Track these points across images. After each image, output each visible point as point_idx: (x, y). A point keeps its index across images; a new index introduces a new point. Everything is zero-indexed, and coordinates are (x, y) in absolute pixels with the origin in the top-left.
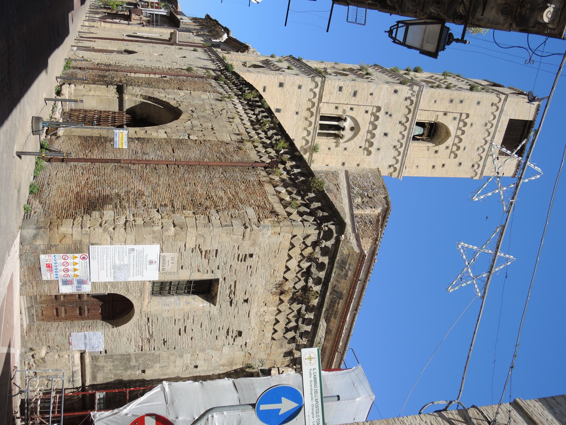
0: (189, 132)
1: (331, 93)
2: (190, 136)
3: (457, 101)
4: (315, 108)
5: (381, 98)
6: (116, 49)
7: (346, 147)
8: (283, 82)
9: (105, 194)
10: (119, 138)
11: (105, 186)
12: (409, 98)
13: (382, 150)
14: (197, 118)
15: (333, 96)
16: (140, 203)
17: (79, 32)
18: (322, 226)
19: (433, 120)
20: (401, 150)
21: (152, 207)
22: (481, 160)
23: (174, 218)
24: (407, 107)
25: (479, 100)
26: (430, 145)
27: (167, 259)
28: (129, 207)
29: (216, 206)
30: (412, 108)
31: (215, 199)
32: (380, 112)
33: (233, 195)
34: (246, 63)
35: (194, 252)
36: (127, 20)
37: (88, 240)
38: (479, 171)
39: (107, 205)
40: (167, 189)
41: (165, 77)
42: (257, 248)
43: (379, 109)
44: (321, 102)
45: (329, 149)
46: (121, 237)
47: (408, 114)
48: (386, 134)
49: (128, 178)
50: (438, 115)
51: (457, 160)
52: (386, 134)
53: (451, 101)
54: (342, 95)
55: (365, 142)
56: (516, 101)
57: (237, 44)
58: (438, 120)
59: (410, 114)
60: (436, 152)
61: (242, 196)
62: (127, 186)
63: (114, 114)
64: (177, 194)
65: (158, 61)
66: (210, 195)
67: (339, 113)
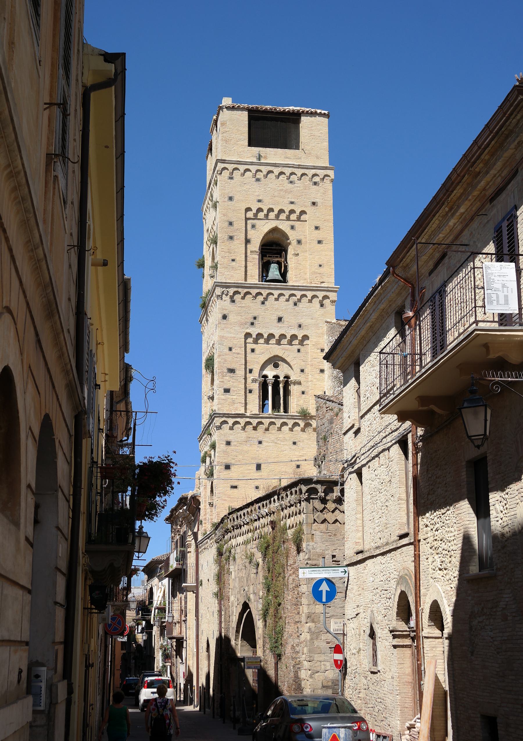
1: (233, 402)
4: (251, 420)
5: (234, 336)
12: (232, 298)
13: (301, 321)
15: (237, 399)
20: (299, 294)
24: (243, 298)
25: (227, 199)
26: (291, 251)
27: (337, 628)
30: (243, 291)
32: (251, 333)
35: (330, 606)
36: (182, 642)
37: (319, 690)
38: (322, 173)
42: (327, 552)
43: (248, 335)
44: (245, 415)
45: (303, 393)
46: (316, 665)
48: (280, 319)
50: (251, 252)
52: (280, 319)
54: (234, 387)
67: (256, 387)
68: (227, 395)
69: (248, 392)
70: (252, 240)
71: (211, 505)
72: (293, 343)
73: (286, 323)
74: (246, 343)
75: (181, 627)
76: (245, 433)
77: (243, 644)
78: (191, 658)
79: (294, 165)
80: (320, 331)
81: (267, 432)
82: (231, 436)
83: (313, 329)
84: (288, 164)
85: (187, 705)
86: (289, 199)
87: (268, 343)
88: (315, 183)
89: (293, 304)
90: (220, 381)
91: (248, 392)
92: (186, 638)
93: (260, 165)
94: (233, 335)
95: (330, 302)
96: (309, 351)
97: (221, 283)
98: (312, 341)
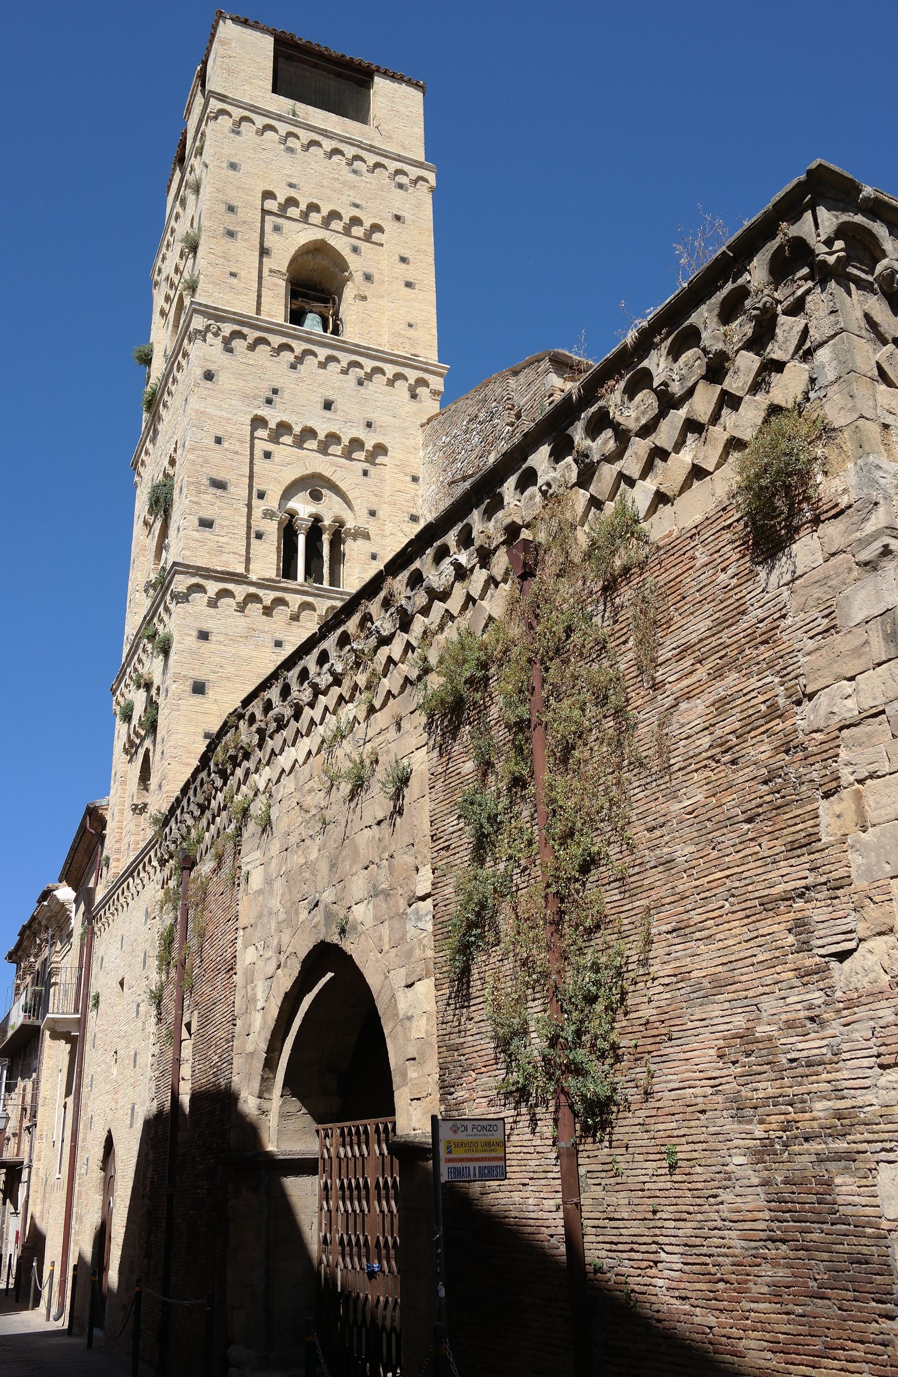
0: (402, 903)
1: (220, 550)
2: (420, 893)
3: (229, 220)
4: (261, 593)
5: (229, 416)
6: (99, 1198)
7: (365, 512)
8: (190, 683)
9: (767, 1215)
10: (471, 1160)
11: (714, 1216)
13: (373, 416)
14: (339, 886)
15: (228, 544)
16: (800, 1046)
17: (48, 1319)
18: (831, 260)
19: (283, 283)
20: (368, 364)
21: (821, 985)
22: (383, 166)
23: (879, 875)
24: (252, 347)
25: (225, 165)
26: (349, 292)
28: (838, 1093)
29: (774, 712)
30: (253, 335)
31: (728, 729)
32: (267, 418)
33: (700, 662)
34: (136, 805)
36: (20, 1172)
38: (414, 172)
39: (840, 1200)
40: (698, 935)
41: (188, 1026)
43: (258, 422)
44: (246, 577)
47: (269, 344)
49: (654, 1112)
50: (271, 271)
51: (389, 225)
52: (328, 405)
53: (231, 234)
54: (224, 518)
55: (354, 462)
56: (224, 75)
57: (81, 849)
58: (284, 270)
59: (269, 339)
60: (368, 277)
61: (701, 625)
62: (703, 1112)
63: (333, 1193)
64: (721, 889)
65: (135, 1062)
66: (709, 754)
67: (271, 528)
68: (206, 533)
69: (253, 535)
70: (274, 251)
71: (138, 811)
72: (354, 456)
73: (340, 413)
74: (253, 438)
75: (19, 1144)
76: (243, 619)
77: (287, 1108)
78: (39, 1201)
79: (361, 142)
80: (411, 442)
81: (295, 623)
82: (211, 620)
83: (396, 435)
84: (350, 139)
85: (27, 1309)
86: (350, 198)
87: (301, 447)
88: (401, 186)
89: (355, 381)
90: (190, 501)
91: (253, 535)
92: (31, 1161)
93: (296, 126)
94: (225, 415)
95: (431, 392)
96: (387, 477)
97: (206, 306)
98: (394, 457)
